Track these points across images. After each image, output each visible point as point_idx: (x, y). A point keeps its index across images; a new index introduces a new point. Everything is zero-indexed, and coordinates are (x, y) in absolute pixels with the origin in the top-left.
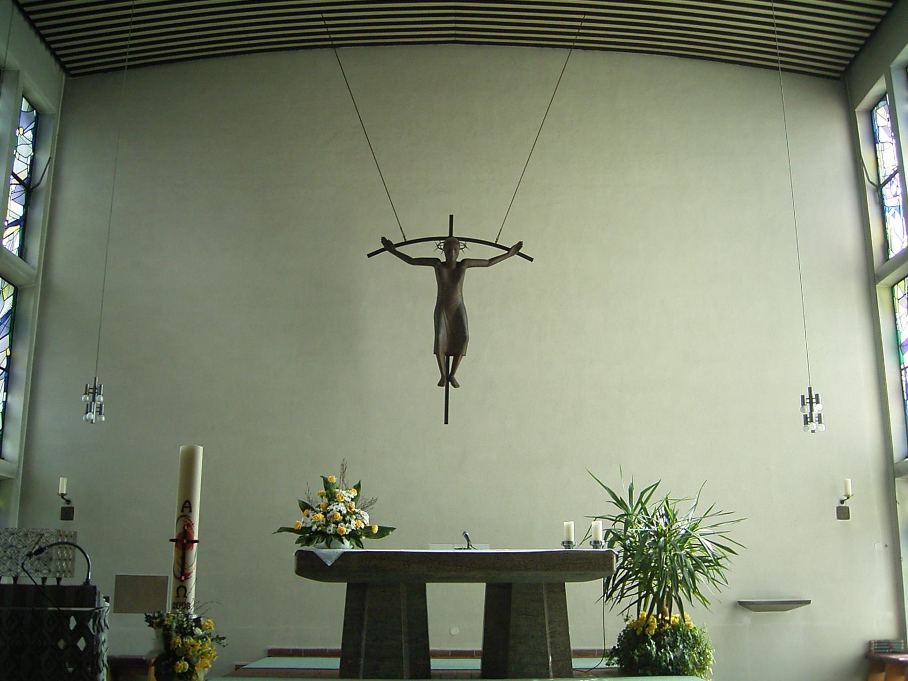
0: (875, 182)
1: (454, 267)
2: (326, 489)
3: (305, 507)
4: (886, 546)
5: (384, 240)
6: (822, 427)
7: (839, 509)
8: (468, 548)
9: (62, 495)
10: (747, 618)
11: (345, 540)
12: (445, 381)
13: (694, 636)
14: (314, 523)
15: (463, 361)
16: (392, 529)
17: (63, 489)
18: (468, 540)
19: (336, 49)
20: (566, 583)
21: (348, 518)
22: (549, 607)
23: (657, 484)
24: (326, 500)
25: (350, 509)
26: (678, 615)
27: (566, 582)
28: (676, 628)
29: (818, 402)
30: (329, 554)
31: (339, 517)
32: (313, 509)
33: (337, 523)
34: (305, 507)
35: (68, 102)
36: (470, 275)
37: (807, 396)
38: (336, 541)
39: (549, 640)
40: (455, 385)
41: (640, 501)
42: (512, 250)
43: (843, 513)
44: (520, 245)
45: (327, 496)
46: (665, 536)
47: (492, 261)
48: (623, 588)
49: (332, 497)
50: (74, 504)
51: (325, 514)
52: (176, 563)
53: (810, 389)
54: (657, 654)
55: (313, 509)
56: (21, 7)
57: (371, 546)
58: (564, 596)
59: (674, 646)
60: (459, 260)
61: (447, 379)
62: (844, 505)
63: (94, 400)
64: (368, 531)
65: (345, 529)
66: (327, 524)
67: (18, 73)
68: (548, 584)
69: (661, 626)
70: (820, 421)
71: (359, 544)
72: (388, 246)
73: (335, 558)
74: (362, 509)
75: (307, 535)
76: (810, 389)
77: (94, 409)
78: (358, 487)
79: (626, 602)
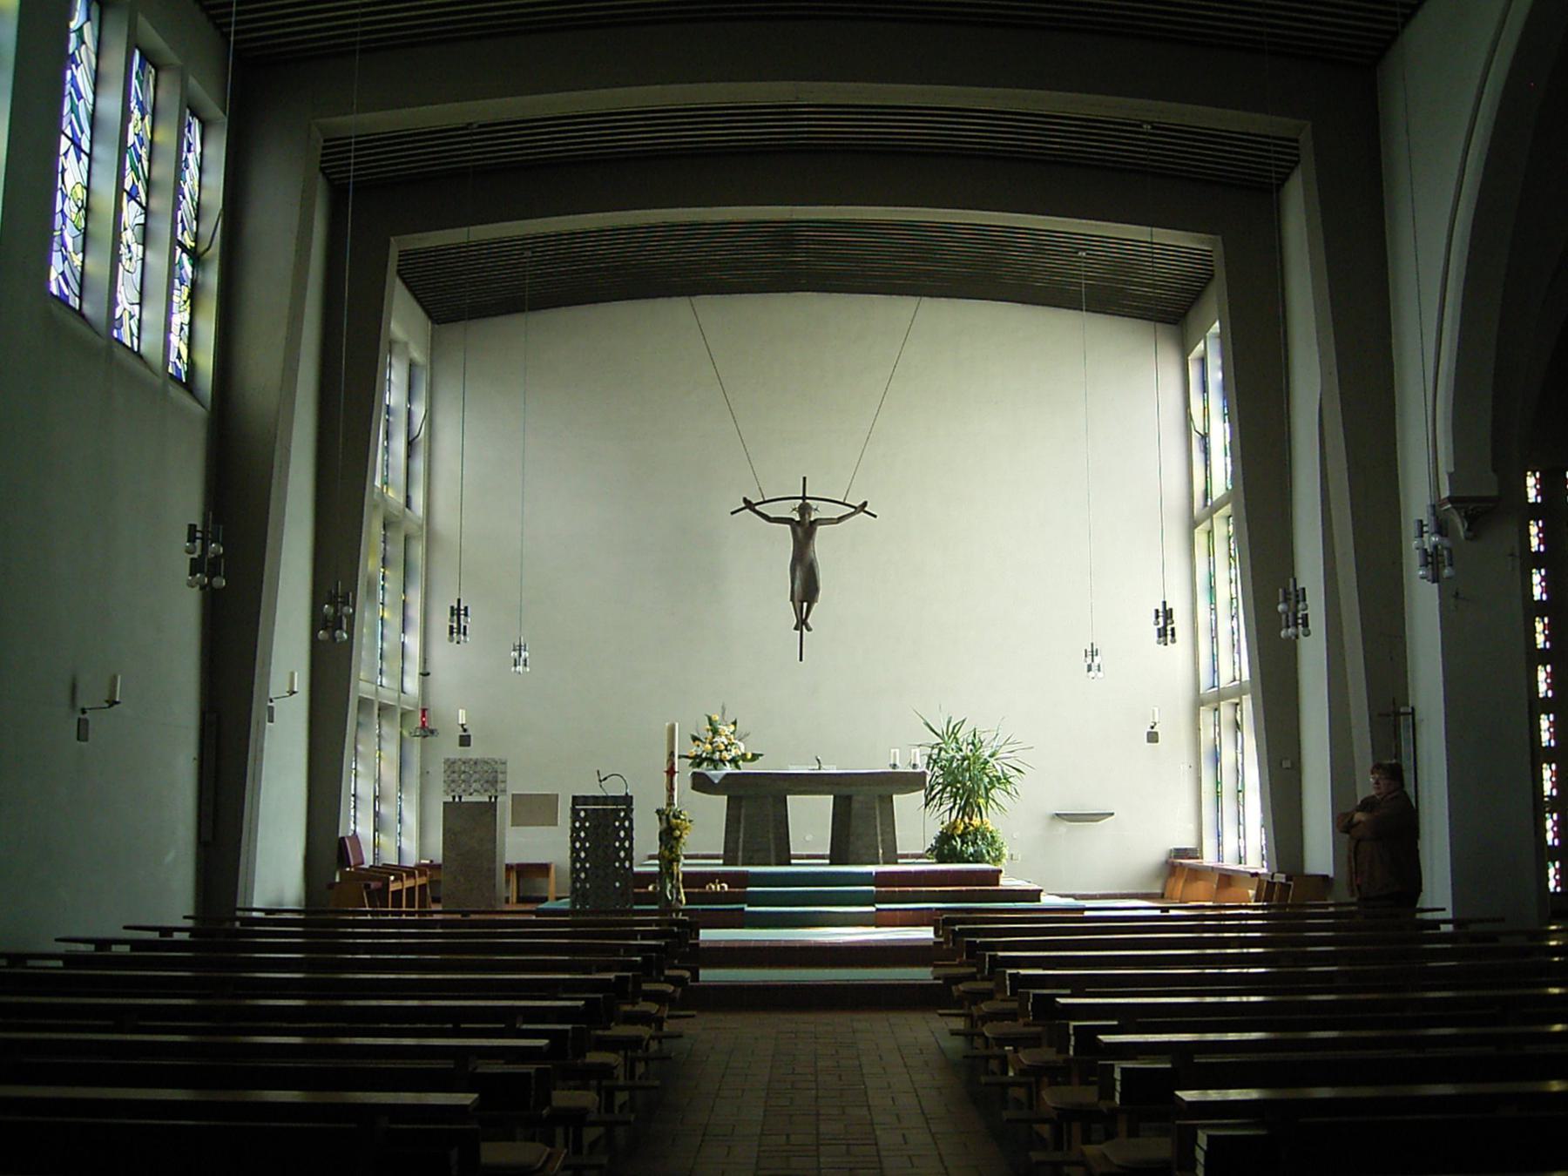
0: (1202, 432)
1: (808, 525)
2: (711, 724)
3: (695, 739)
4: (1190, 767)
5: (745, 500)
6: (1100, 675)
7: (1149, 733)
8: (819, 769)
9: (462, 725)
10: (1064, 827)
11: (727, 764)
12: (800, 625)
13: (992, 837)
14: (703, 751)
15: (815, 607)
16: (761, 755)
17: (462, 720)
18: (819, 763)
19: (693, 299)
20: (788, 797)
21: (729, 747)
22: (881, 813)
23: (964, 721)
24: (710, 733)
25: (730, 740)
26: (979, 818)
27: (790, 794)
28: (977, 829)
29: (1097, 655)
30: (716, 774)
31: (723, 747)
32: (701, 741)
33: (721, 751)
34: (695, 739)
35: (435, 349)
36: (820, 530)
37: (1090, 649)
38: (721, 765)
39: (879, 838)
40: (809, 629)
41: (953, 732)
42: (858, 509)
43: (1153, 737)
44: (865, 504)
45: (712, 730)
46: (969, 760)
47: (841, 519)
48: (941, 798)
49: (715, 732)
50: (470, 732)
51: (711, 744)
52: (1337, 830)
53: (1092, 645)
54: (961, 849)
55: (701, 741)
56: (206, 9)
57: (746, 768)
58: (890, 804)
59: (974, 843)
60: (812, 519)
61: (802, 624)
62: (1154, 730)
63: (520, 655)
64: (743, 757)
65: (727, 756)
66: (713, 753)
67: (406, 344)
68: (880, 796)
69: (966, 828)
70: (1099, 670)
71: (738, 767)
72: (749, 505)
73: (720, 777)
74: (740, 740)
75: (698, 760)
76: (1092, 645)
77: (522, 663)
78: (735, 723)
79: (943, 808)
